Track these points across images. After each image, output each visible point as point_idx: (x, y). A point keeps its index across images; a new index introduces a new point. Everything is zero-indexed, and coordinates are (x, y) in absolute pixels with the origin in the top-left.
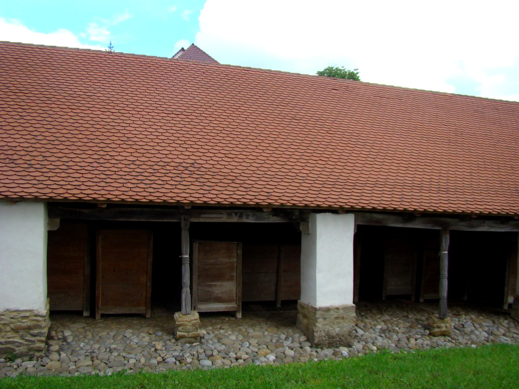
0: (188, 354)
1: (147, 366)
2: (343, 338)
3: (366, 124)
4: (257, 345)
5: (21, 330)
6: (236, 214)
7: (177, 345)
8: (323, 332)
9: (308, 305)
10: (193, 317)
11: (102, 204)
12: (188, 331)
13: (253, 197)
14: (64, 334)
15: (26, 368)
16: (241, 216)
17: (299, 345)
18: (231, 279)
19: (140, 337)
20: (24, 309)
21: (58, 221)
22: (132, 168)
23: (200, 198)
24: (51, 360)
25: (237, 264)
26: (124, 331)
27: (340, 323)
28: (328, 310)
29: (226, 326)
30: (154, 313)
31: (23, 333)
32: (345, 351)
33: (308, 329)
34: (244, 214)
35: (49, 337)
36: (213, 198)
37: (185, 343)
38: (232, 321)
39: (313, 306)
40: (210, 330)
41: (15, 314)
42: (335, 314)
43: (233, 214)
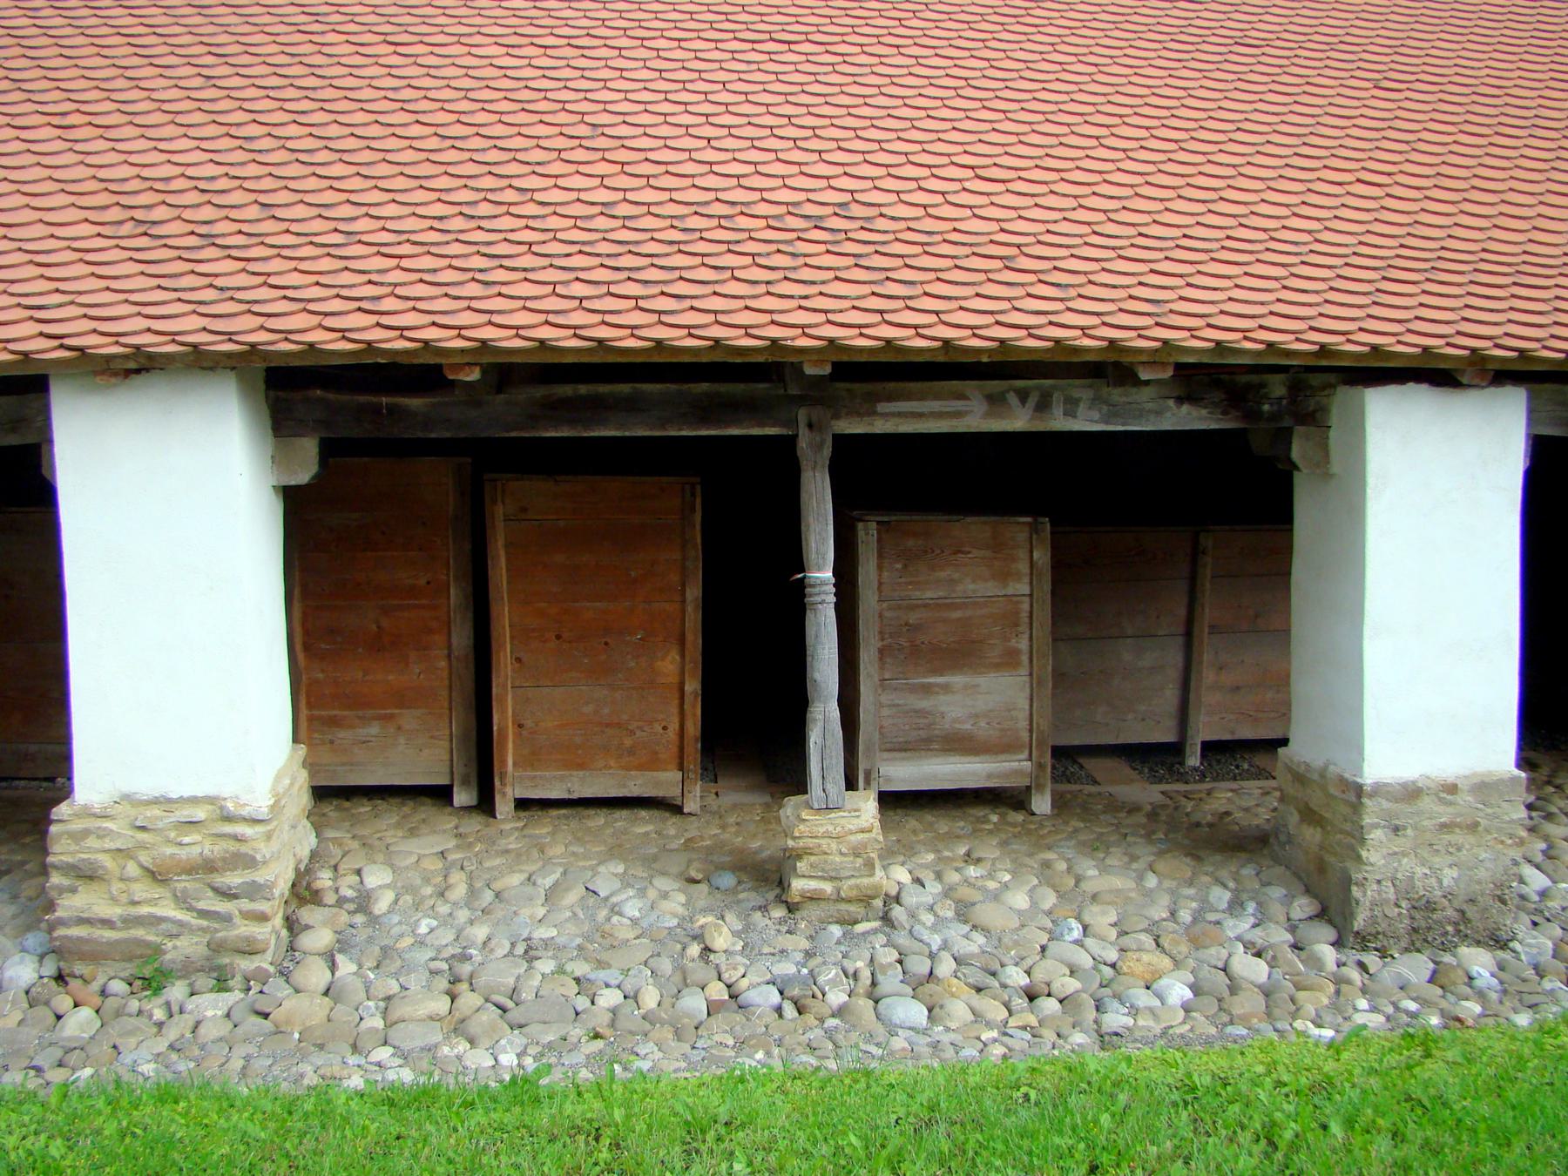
0: (834, 972)
1: (662, 1025)
2: (1471, 912)
3: (1455, 142)
4: (1113, 933)
5: (179, 874)
6: (1023, 396)
7: (789, 932)
8: (1390, 884)
9: (1323, 773)
10: (855, 821)
11: (460, 367)
12: (833, 874)
13: (1095, 321)
14: (362, 882)
15: (197, 1024)
16: (1043, 406)
17: (1289, 937)
18: (1009, 661)
19: (652, 894)
20: (186, 794)
21: (309, 448)
22: (597, 231)
23: (867, 326)
24: (297, 991)
25: (1031, 606)
26: (593, 868)
27: (1459, 850)
28: (1411, 793)
29: (989, 850)
30: (717, 794)
31: (187, 884)
32: (1479, 962)
33: (1322, 868)
34: (1055, 395)
35: (303, 892)
36: (924, 327)
37: (825, 922)
38: (1014, 825)
39: (1347, 775)
40: (926, 866)
41: (156, 811)
42: (1441, 809)
43: (1013, 399)
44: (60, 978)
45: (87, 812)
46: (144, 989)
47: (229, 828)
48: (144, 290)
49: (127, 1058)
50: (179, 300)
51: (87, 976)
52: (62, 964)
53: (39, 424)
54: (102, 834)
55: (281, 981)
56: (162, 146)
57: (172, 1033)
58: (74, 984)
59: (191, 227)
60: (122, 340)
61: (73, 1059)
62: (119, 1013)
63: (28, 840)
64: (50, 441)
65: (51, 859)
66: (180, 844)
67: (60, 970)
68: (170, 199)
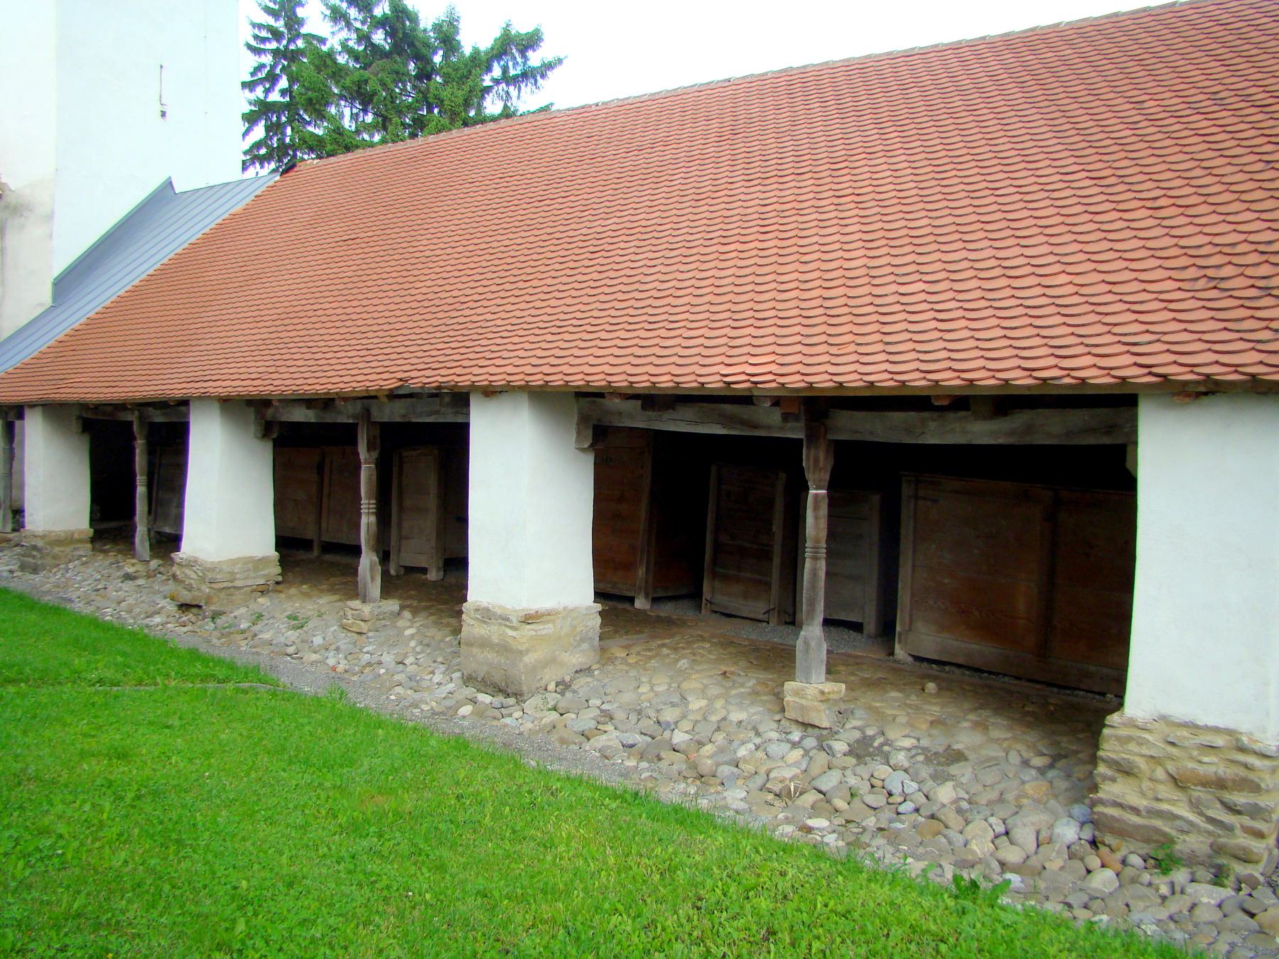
5: (1196, 785)
15: (1193, 907)
41: (1185, 733)
44: (1094, 843)
45: (1132, 723)
46: (1155, 867)
47: (1241, 757)
48: (1214, 331)
49: (1135, 916)
50: (1241, 339)
51: (1113, 847)
52: (1097, 833)
53: (1126, 430)
54: (1141, 742)
55: (1269, 891)
56: (1230, 218)
57: (1173, 907)
58: (1104, 850)
59: (1250, 282)
60: (1197, 370)
61: (1096, 905)
62: (1134, 881)
63: (1081, 736)
64: (1136, 443)
65: (1100, 753)
66: (1200, 762)
67: (1094, 836)
68: (1235, 260)
